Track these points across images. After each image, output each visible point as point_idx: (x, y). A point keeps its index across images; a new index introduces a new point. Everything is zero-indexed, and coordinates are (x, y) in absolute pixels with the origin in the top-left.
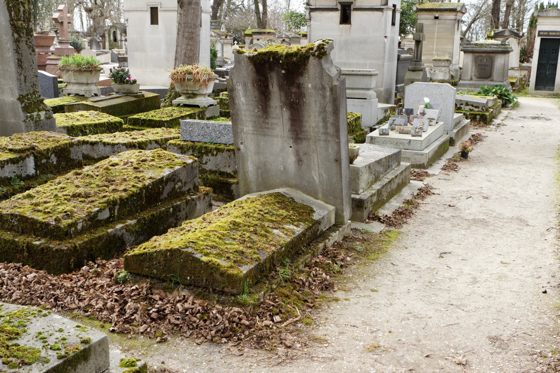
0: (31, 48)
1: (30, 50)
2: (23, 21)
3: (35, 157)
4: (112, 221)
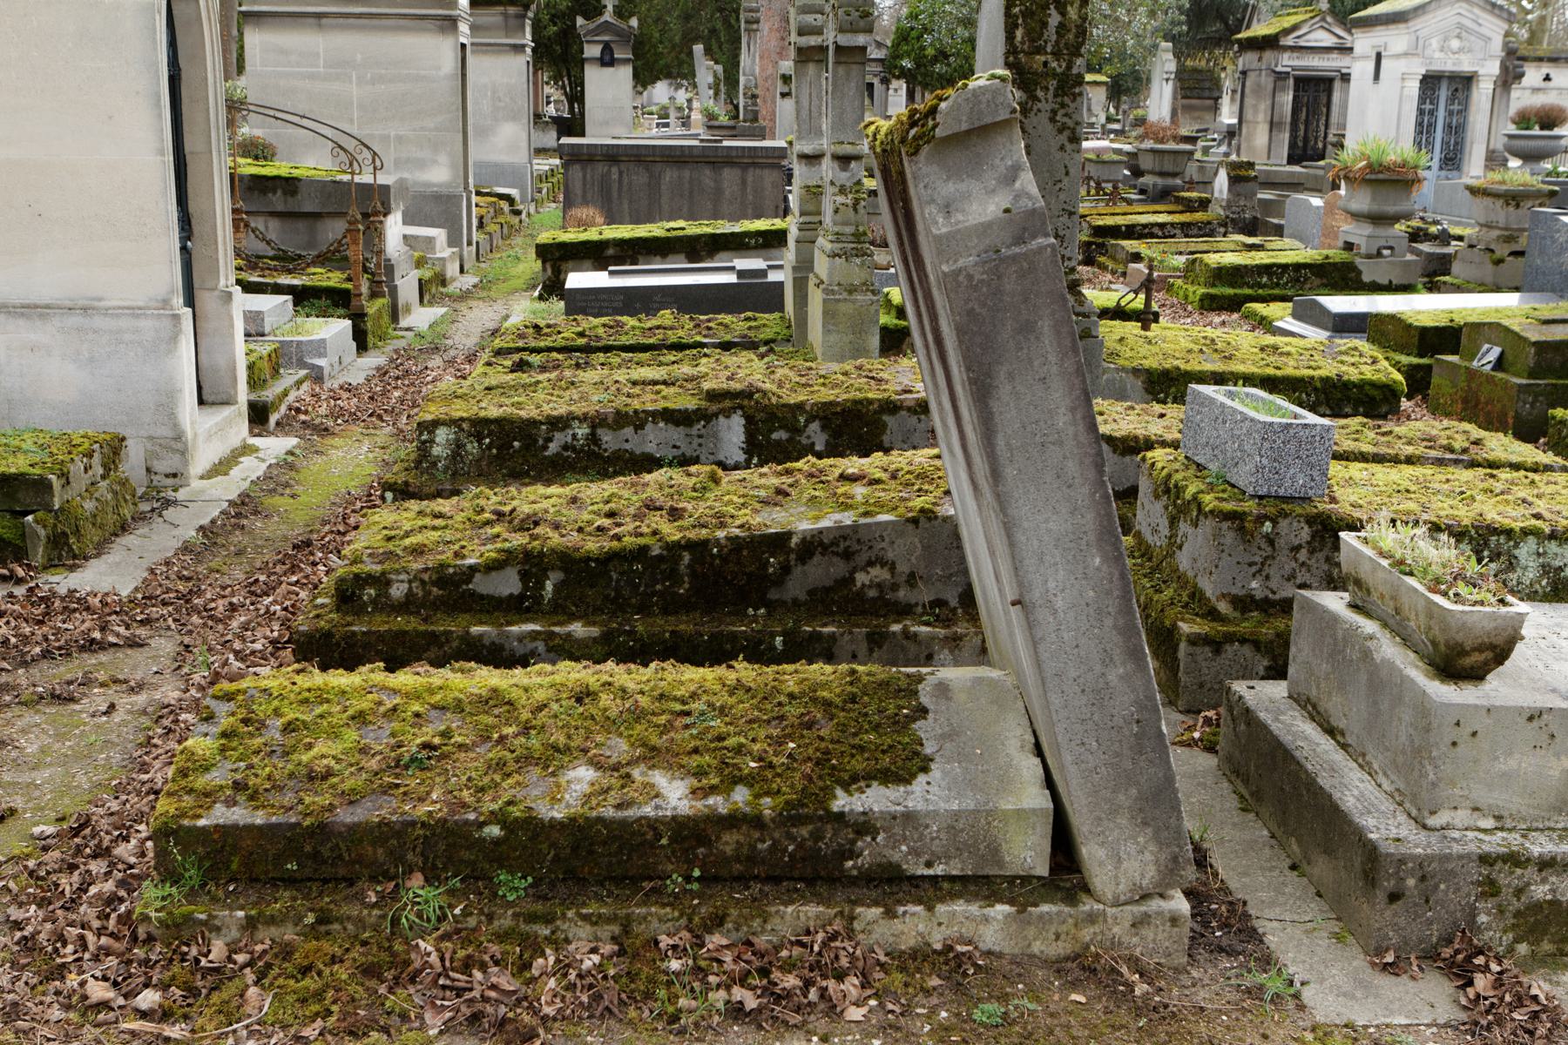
0: (1067, 133)
1: (1063, 138)
2: (1053, 53)
3: (750, 420)
4: (528, 610)
